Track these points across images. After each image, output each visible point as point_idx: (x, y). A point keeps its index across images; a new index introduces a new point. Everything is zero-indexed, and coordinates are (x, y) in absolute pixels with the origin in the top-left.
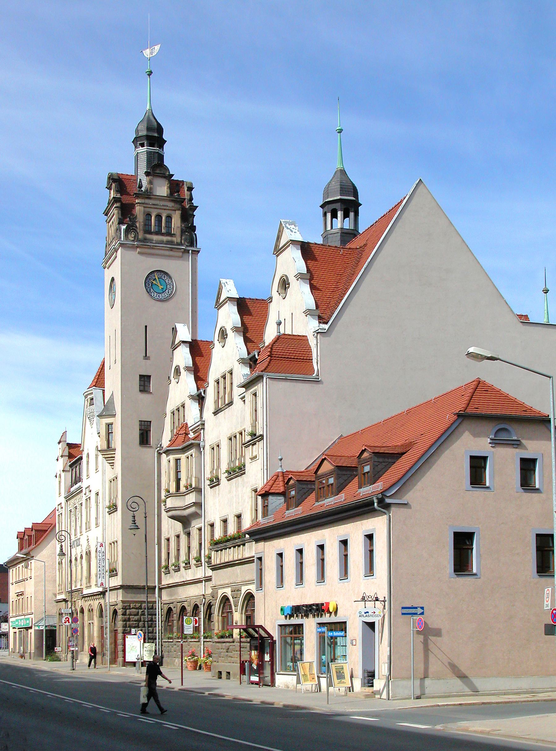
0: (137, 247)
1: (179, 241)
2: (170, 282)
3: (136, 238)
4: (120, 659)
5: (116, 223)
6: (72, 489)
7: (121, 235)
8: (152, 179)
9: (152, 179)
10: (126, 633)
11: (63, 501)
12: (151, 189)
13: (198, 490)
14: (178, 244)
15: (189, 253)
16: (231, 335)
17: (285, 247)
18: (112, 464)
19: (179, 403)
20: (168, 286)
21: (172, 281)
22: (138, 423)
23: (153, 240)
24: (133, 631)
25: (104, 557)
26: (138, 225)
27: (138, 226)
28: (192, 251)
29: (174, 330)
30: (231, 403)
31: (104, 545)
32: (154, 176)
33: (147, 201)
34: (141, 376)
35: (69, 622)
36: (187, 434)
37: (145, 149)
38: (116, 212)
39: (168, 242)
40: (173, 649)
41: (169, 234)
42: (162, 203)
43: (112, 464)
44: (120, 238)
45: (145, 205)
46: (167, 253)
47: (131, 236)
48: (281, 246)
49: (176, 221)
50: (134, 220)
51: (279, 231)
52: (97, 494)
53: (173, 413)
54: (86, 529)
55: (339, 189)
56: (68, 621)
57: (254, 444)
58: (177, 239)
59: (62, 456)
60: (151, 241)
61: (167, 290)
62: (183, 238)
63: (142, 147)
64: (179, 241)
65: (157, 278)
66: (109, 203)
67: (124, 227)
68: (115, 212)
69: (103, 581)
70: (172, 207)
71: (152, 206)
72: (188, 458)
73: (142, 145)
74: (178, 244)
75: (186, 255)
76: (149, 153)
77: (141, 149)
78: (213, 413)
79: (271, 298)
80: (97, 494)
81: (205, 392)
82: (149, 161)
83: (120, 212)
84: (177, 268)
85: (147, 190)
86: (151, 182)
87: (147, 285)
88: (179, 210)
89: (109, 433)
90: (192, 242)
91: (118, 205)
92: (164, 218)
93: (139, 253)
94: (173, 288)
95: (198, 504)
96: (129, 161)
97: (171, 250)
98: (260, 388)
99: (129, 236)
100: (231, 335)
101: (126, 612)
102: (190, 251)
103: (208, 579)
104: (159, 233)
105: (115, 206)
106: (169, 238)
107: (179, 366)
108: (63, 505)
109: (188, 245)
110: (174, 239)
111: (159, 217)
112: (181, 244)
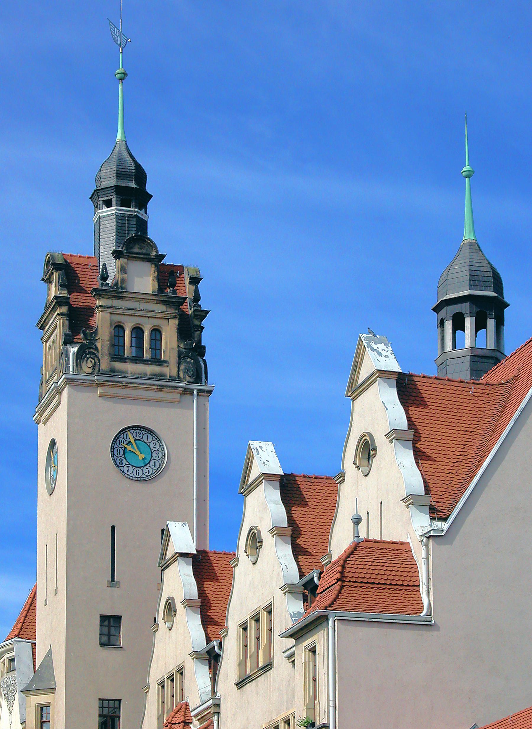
0: (99, 385)
1: (174, 373)
2: (158, 446)
3: (96, 369)
5: (60, 340)
7: (68, 363)
9: (127, 264)
12: (123, 281)
14: (172, 379)
17: (256, 483)
20: (154, 455)
21: (161, 446)
22: (97, 704)
23: (126, 372)
26: (99, 345)
28: (199, 391)
29: (165, 534)
32: (129, 258)
33: (116, 303)
34: (104, 618)
37: (113, 210)
38: (59, 322)
41: (156, 361)
42: (144, 306)
44: (68, 368)
45: (111, 311)
47: (87, 366)
48: (360, 381)
50: (92, 336)
51: (358, 355)
53: (162, 685)
55: (467, 278)
58: (171, 370)
60: (123, 373)
61: (152, 463)
62: (182, 367)
64: (174, 373)
66: (47, 307)
68: (58, 325)
70: (162, 312)
71: (126, 312)
73: (108, 204)
74: (172, 379)
75: (189, 397)
76: (120, 219)
77: (105, 211)
78: (237, 685)
81: (220, 645)
82: (120, 231)
83: (67, 322)
85: (116, 284)
86: (123, 270)
88: (174, 318)
89: (42, 723)
90: (198, 375)
91: (64, 309)
92: (147, 334)
93: (101, 396)
94: (163, 458)
97: (161, 390)
99: (84, 365)
102: (195, 392)
104: (138, 359)
106: (156, 369)
109: (192, 380)
110: (165, 370)
111: (138, 331)
112: (178, 379)
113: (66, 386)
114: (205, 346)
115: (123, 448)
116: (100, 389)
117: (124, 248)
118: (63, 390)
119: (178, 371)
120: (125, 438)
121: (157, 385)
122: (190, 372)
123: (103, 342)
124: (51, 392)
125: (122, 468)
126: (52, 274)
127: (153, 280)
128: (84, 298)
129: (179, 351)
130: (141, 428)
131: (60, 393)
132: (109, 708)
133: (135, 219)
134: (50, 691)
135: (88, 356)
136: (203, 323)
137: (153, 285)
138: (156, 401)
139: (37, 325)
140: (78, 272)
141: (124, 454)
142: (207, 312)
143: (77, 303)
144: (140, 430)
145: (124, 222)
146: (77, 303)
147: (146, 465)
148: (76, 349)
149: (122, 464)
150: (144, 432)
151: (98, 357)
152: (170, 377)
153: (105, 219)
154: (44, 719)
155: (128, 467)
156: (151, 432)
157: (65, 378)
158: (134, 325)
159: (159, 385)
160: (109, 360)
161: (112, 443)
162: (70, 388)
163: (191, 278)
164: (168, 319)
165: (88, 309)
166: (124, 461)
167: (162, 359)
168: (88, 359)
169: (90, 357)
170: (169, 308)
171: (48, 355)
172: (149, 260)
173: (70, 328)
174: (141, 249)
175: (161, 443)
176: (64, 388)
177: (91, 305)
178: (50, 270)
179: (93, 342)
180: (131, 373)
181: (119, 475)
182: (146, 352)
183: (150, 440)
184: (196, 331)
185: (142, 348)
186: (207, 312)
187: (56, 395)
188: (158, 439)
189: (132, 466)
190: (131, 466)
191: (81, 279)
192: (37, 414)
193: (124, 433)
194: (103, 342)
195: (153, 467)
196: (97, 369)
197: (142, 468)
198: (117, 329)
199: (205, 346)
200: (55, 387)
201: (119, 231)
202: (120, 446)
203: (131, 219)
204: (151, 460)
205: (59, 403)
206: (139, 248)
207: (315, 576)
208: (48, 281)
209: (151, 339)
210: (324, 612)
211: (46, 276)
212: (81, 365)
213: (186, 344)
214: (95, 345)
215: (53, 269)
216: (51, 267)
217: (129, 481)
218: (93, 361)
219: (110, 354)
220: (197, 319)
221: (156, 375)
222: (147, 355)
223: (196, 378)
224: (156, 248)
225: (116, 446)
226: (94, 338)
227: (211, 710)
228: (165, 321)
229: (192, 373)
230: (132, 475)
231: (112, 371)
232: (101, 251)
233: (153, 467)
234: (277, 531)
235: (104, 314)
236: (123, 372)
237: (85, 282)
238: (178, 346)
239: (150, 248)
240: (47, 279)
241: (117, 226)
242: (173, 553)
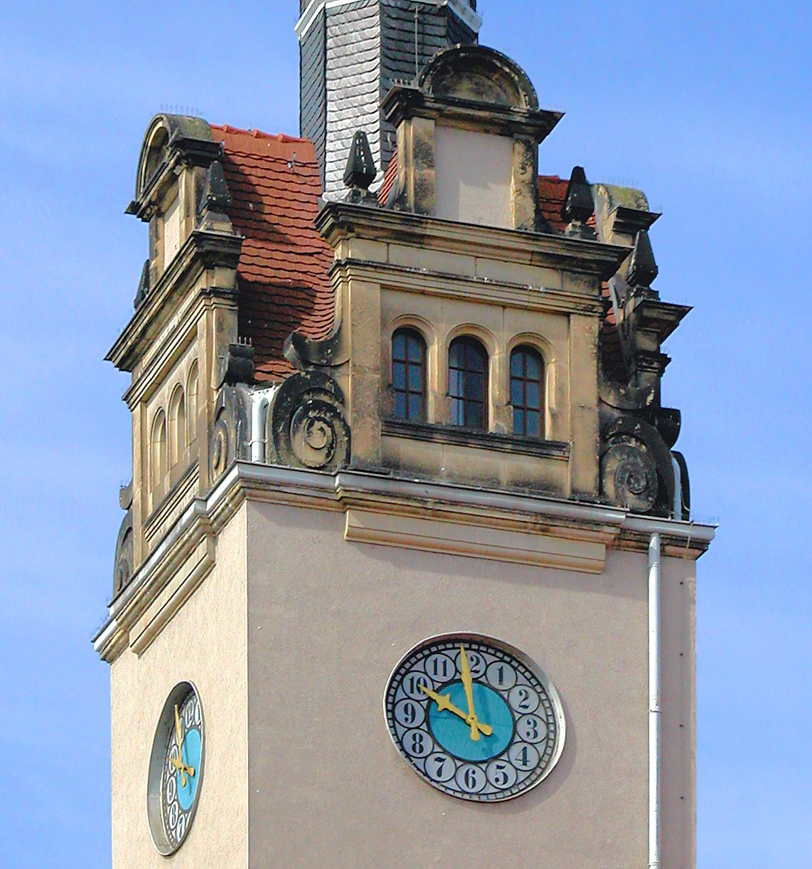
0: (346, 503)
1: (587, 481)
2: (533, 701)
5: (209, 375)
7: (244, 433)
8: (433, 137)
9: (433, 137)
12: (422, 188)
15: (644, 548)
20: (523, 728)
21: (545, 701)
23: (434, 471)
27: (348, 393)
28: (669, 541)
32: (442, 118)
33: (401, 254)
38: (206, 320)
39: (523, 487)
44: (244, 450)
47: (309, 444)
49: (572, 383)
50: (321, 360)
58: (577, 471)
60: (423, 473)
61: (516, 751)
62: (612, 465)
64: (587, 481)
65: (467, 678)
66: (143, 302)
67: (260, 399)
70: (550, 293)
71: (432, 285)
83: (232, 320)
84: (585, 633)
85: (401, 199)
88: (588, 311)
90: (664, 489)
91: (223, 278)
93: (355, 538)
94: (550, 739)
97: (545, 531)
99: (298, 442)
104: (470, 430)
105: (202, 284)
106: (530, 466)
109: (644, 505)
110: (558, 471)
111: (469, 351)
113: (238, 505)
114: (675, 414)
115: (425, 703)
116: (350, 519)
117: (426, 85)
118: (224, 523)
119: (601, 475)
120: (431, 673)
121: (537, 514)
122: (637, 481)
123: (359, 375)
124: (179, 537)
125: (420, 763)
126: (173, 179)
127: (519, 192)
128: (280, 256)
129: (602, 416)
130: (480, 644)
131: (214, 535)
133: (441, 21)
135: (311, 414)
136: (665, 348)
137: (519, 209)
138: (529, 562)
139: (109, 358)
140: (254, 180)
141: (427, 720)
142: (681, 311)
143: (256, 270)
144: (478, 651)
145: (408, 26)
146: (256, 270)
147: (496, 758)
148: (270, 395)
149: (421, 750)
150: (490, 659)
151: (343, 420)
152: (574, 491)
153: (342, 18)
155: (526, 707)
156: (513, 659)
157: (240, 477)
158: (456, 329)
159: (543, 515)
160: (378, 431)
161: (390, 687)
162: (257, 514)
163: (622, 212)
164: (568, 315)
165: (296, 289)
166: (428, 743)
167: (548, 435)
168: (311, 425)
169: (319, 419)
170: (572, 280)
171: (153, 442)
172: (508, 130)
173: (243, 331)
174: (480, 93)
175: (544, 691)
176: (232, 513)
177: (301, 276)
178: (164, 166)
179: (328, 371)
180: (449, 476)
181: (413, 784)
182: (497, 414)
183: (508, 684)
184: (643, 369)
185: (483, 398)
186: (681, 311)
187: (197, 543)
188: (536, 682)
189: (454, 757)
190: (448, 759)
191: (265, 200)
192: (114, 623)
193: (426, 657)
194: (359, 375)
195: (519, 764)
196: (340, 455)
197: (484, 766)
198: (401, 339)
199: (675, 414)
200: (197, 515)
201: (389, 53)
202: (416, 695)
203: (430, 19)
204: (511, 743)
205: (208, 567)
206: (472, 90)
208: (149, 210)
209: (512, 378)
211: (146, 193)
212: (288, 441)
213: (626, 396)
214: (334, 383)
215: (177, 163)
216: (173, 153)
217: (448, 803)
218: (328, 431)
219: (381, 413)
220: (646, 333)
221: (526, 484)
222: (496, 422)
223: (657, 500)
224: (530, 90)
225: (400, 695)
226: (329, 361)
228: (560, 322)
229: (643, 483)
230: (452, 785)
231: (389, 467)
232: (330, 117)
233: (519, 764)
235: (363, 287)
236: (421, 471)
237: (280, 212)
238: (600, 401)
239: (510, 91)
240: (150, 203)
241: (385, 37)
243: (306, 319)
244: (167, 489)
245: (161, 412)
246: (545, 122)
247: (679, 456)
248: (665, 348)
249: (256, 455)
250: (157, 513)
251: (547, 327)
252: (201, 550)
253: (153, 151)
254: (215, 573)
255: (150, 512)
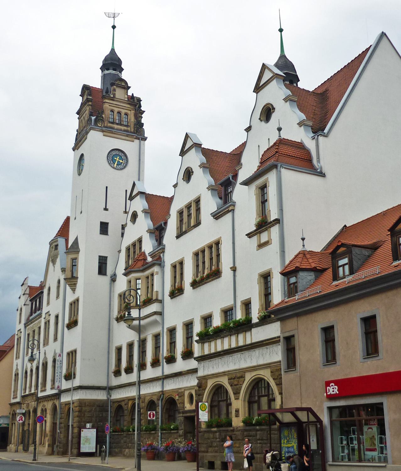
4: (75, 451)
6: (31, 318)
10: (81, 427)
11: (22, 326)
13: (161, 302)
16: (141, 216)
17: (137, 195)
18: (74, 290)
19: (135, 238)
24: (88, 425)
25: (61, 365)
30: (198, 223)
31: (61, 355)
35: (22, 420)
36: (145, 259)
39: (125, 131)
40: (122, 441)
43: (74, 290)
44: (91, 124)
45: (109, 104)
46: (124, 137)
52: (57, 317)
54: (16, 358)
56: (22, 419)
57: (260, 233)
59: (24, 294)
63: (107, 70)
67: (93, 118)
69: (60, 385)
72: (148, 277)
74: (131, 132)
79: (126, 224)
80: (57, 317)
87: (109, 158)
88: (133, 110)
89: (73, 266)
95: (160, 314)
96: (96, 81)
98: (271, 178)
100: (141, 216)
101: (82, 409)
103: (195, 371)
107: (136, 212)
108: (22, 330)
114: (143, 124)
119: (134, 130)
126: (85, 92)
132: (102, 260)
134: (77, 252)
141: (112, 159)
142: (144, 111)
154: (74, 264)
181: (110, 167)
186: (144, 111)
199: (143, 124)
207: (230, 177)
210: (275, 163)
227: (230, 208)
234: (145, 211)
242: (137, 192)
243: (45, 353)
244: (82, 129)
245: (82, 120)
246: (129, 88)
247: (144, 129)
248: (142, 116)
249: (93, 124)
250: (81, 132)
251: (129, 112)
252: (86, 136)
253: (83, 89)
254: (87, 139)
255: (80, 132)
